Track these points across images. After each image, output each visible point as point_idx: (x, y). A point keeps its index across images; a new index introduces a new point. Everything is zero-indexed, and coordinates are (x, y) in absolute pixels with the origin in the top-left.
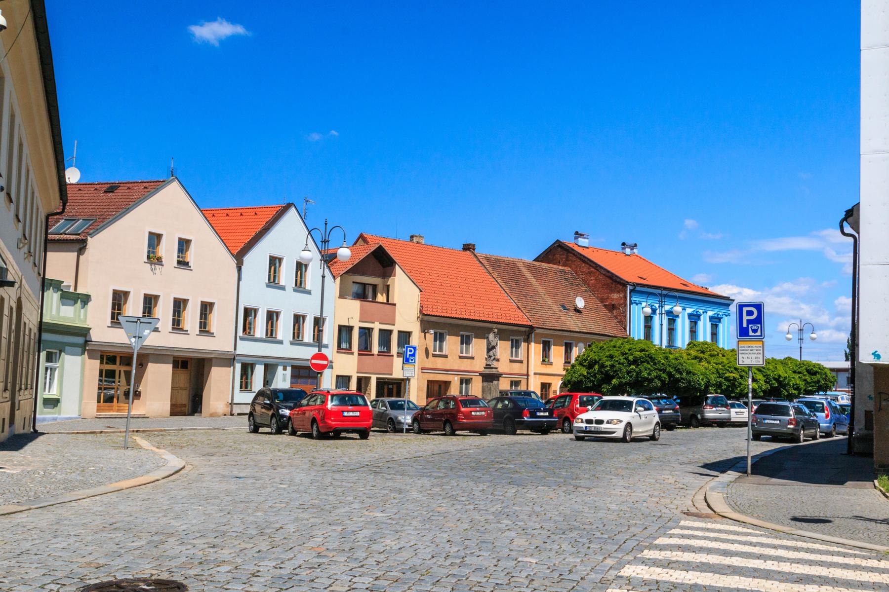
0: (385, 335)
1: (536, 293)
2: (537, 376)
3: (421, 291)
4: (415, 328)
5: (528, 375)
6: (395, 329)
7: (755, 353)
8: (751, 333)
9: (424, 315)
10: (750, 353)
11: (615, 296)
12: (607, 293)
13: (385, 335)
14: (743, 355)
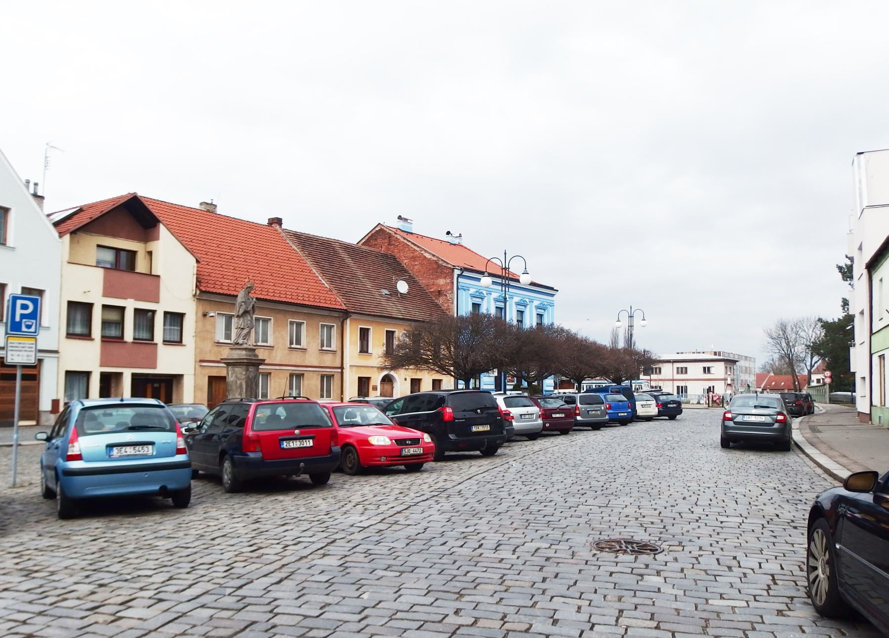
0: (145, 318)
1: (354, 276)
2: (354, 368)
3: (198, 262)
4: (188, 306)
5: (342, 368)
6: (160, 309)
7: (26, 351)
8: (24, 329)
9: (201, 291)
10: (21, 351)
11: (441, 282)
12: (433, 279)
13: (145, 318)
14: (12, 352)
